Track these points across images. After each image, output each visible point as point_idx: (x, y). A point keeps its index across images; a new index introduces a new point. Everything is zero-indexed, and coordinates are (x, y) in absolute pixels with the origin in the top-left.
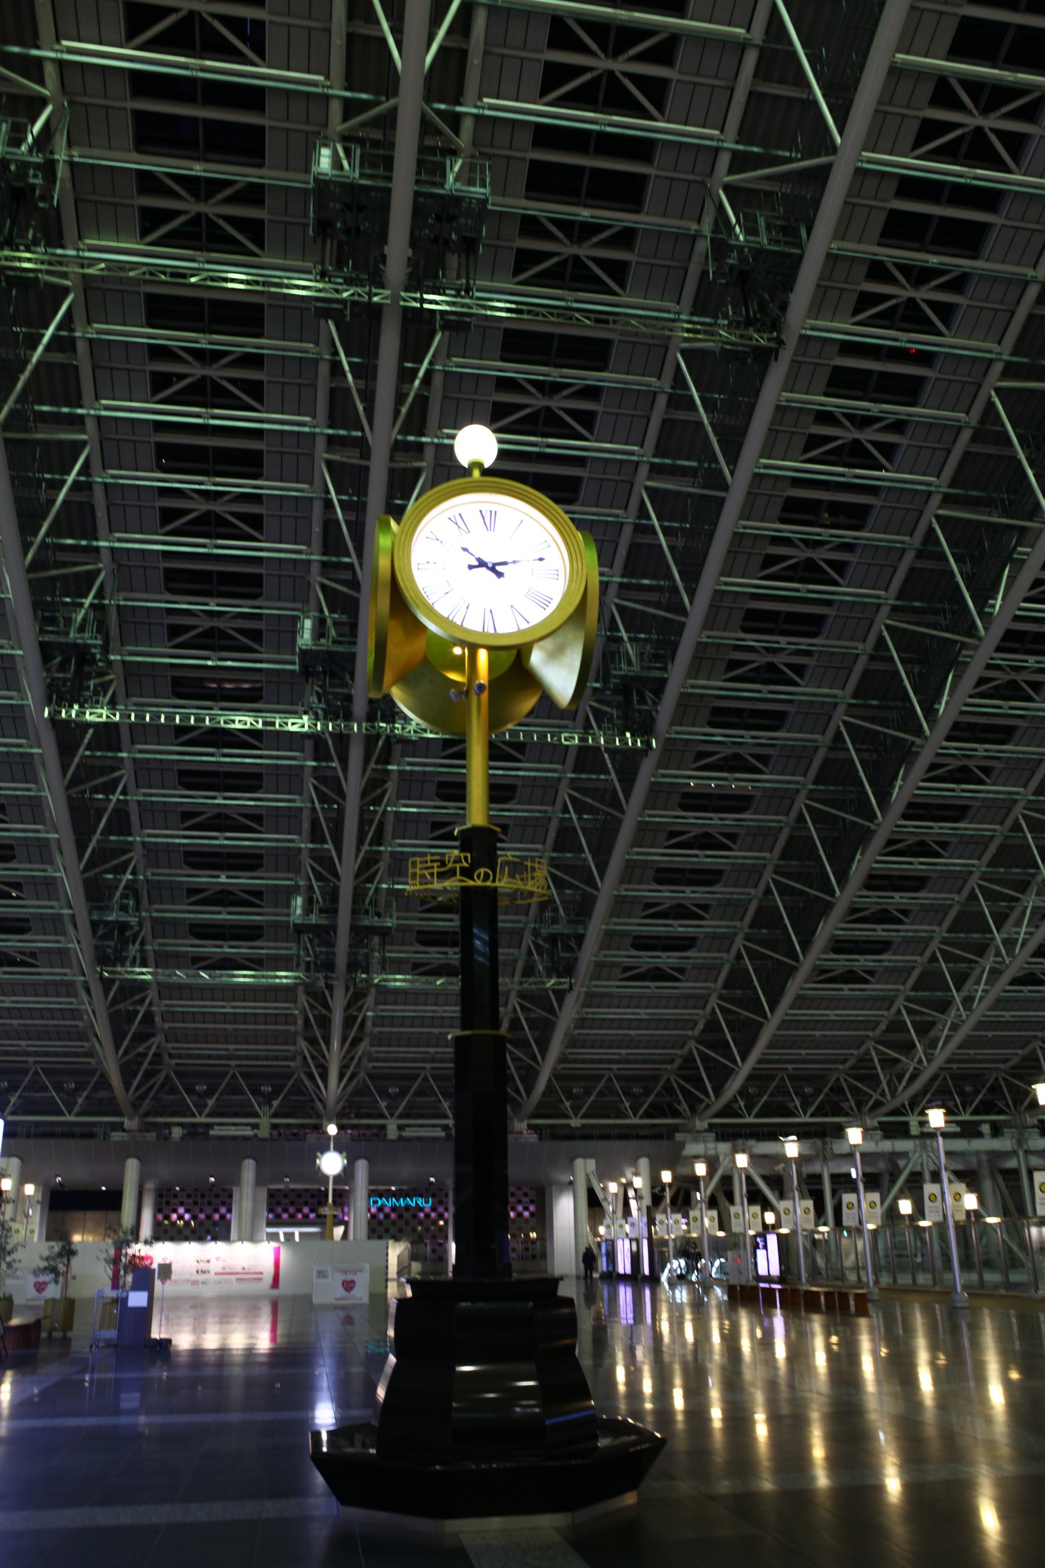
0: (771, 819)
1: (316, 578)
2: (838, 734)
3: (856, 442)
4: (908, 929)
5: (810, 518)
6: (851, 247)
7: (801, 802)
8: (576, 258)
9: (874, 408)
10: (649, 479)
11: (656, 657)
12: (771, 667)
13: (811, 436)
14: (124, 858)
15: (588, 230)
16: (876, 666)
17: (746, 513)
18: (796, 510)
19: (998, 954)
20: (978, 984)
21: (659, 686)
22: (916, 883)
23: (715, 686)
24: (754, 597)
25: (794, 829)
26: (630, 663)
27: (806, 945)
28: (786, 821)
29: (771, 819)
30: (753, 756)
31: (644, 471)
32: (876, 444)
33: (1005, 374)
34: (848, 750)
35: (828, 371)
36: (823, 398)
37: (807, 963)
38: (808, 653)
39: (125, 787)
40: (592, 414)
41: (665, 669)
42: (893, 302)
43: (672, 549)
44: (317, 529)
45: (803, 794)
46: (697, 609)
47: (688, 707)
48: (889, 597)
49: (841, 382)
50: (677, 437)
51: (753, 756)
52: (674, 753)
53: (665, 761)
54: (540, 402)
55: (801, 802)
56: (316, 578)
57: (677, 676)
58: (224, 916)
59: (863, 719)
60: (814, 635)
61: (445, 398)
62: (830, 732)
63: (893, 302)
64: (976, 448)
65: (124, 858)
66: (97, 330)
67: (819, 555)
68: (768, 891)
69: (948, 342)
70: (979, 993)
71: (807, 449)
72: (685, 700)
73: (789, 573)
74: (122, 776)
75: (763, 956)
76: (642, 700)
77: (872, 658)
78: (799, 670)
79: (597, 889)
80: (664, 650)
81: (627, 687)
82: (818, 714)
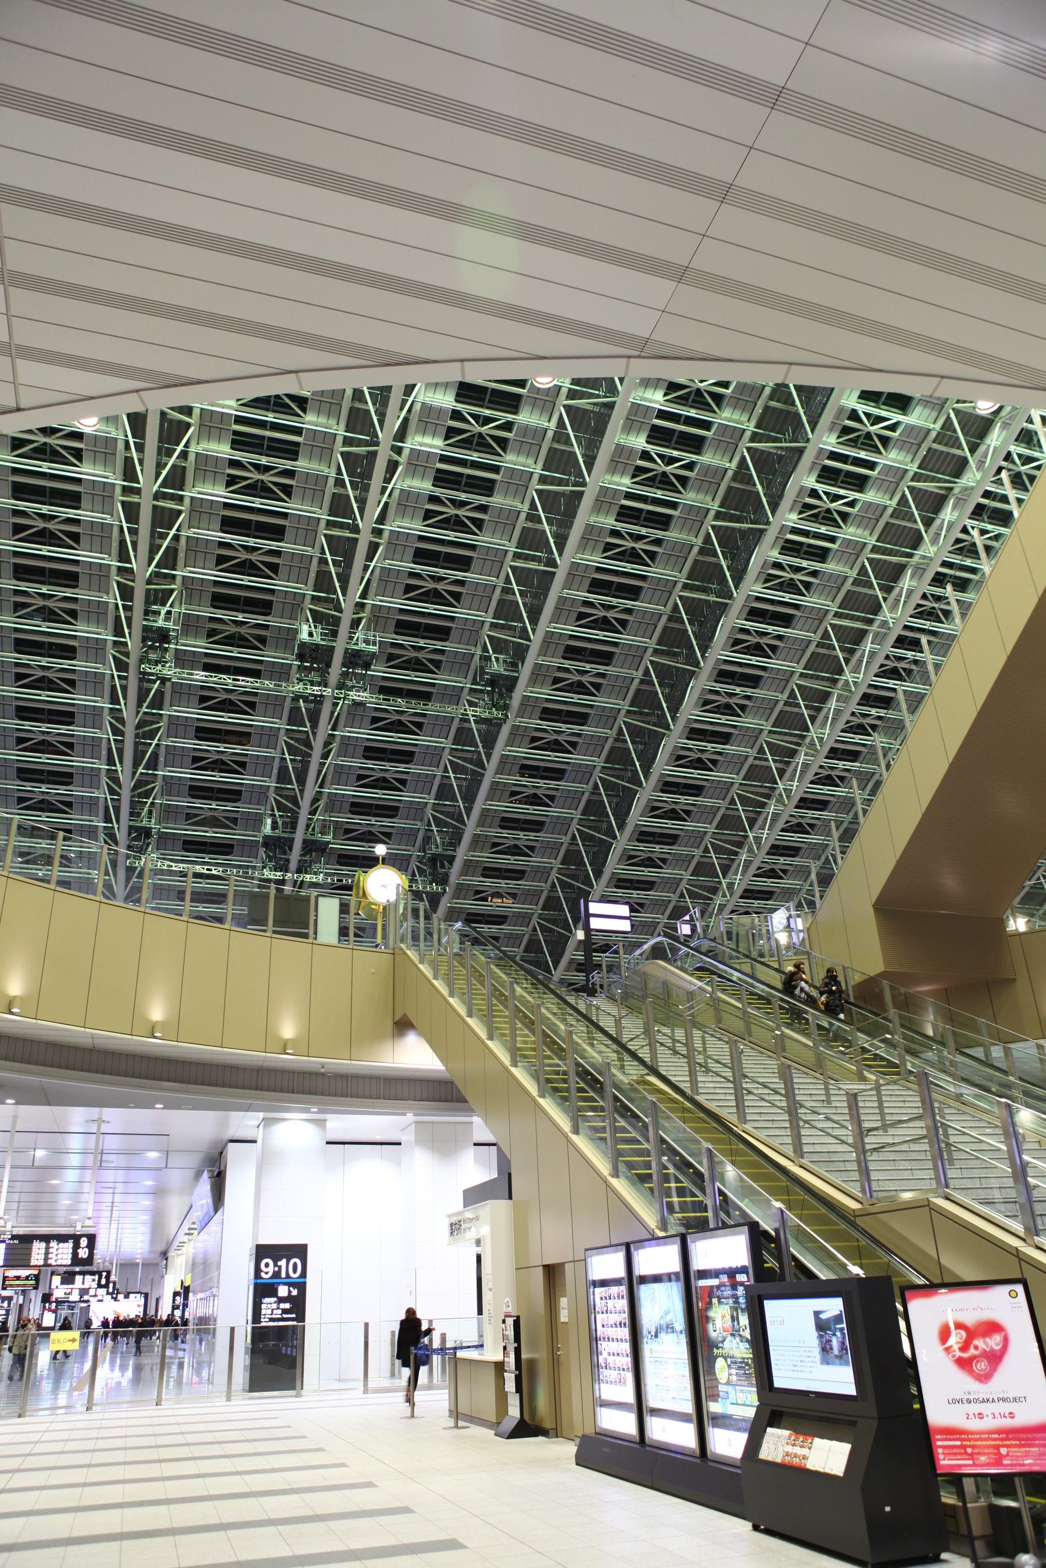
0: (518, 930)
1: (272, 795)
2: (574, 836)
3: (633, 548)
4: (667, 872)
5: (581, 657)
6: (504, 779)
7: (535, 920)
8: (457, 516)
9: (615, 601)
10: (513, 561)
11: (451, 844)
12: (556, 742)
13: (608, 543)
14: (155, 726)
15: (463, 504)
16: (618, 745)
17: (568, 585)
18: (571, 652)
19: (724, 896)
20: (763, 829)
21: (451, 860)
22: (671, 839)
23: (544, 692)
24: (547, 700)
25: (531, 935)
26: (437, 847)
27: (556, 963)
28: (527, 931)
29: (518, 930)
30: (525, 846)
31: (487, 626)
32: (645, 551)
33: (752, 440)
34: (600, 794)
35: (589, 580)
36: (539, 722)
37: (707, 666)
38: (579, 735)
39: (180, 526)
40: (440, 661)
41: (455, 850)
42: (688, 390)
43: (524, 604)
44: (275, 771)
45: (536, 915)
46: (536, 640)
47: (468, 867)
48: (652, 644)
49: (596, 586)
50: (506, 610)
51: (525, 846)
52: (461, 891)
53: (456, 895)
54: (452, 511)
55: (535, 920)
56: (272, 795)
57: (461, 854)
58: (210, 833)
59: (612, 776)
60: (607, 665)
61: (349, 713)
62: (549, 882)
63: (688, 390)
64: (700, 558)
65: (155, 726)
66: (192, 532)
67: (585, 679)
68: (553, 885)
69: (654, 571)
70: (765, 836)
71: (578, 620)
72: (504, 759)
73: (593, 625)
74: (159, 728)
75: (571, 886)
76: (443, 866)
77: (592, 793)
78: (574, 745)
79: (465, 825)
80: (455, 839)
81: (434, 860)
82: (609, 717)
